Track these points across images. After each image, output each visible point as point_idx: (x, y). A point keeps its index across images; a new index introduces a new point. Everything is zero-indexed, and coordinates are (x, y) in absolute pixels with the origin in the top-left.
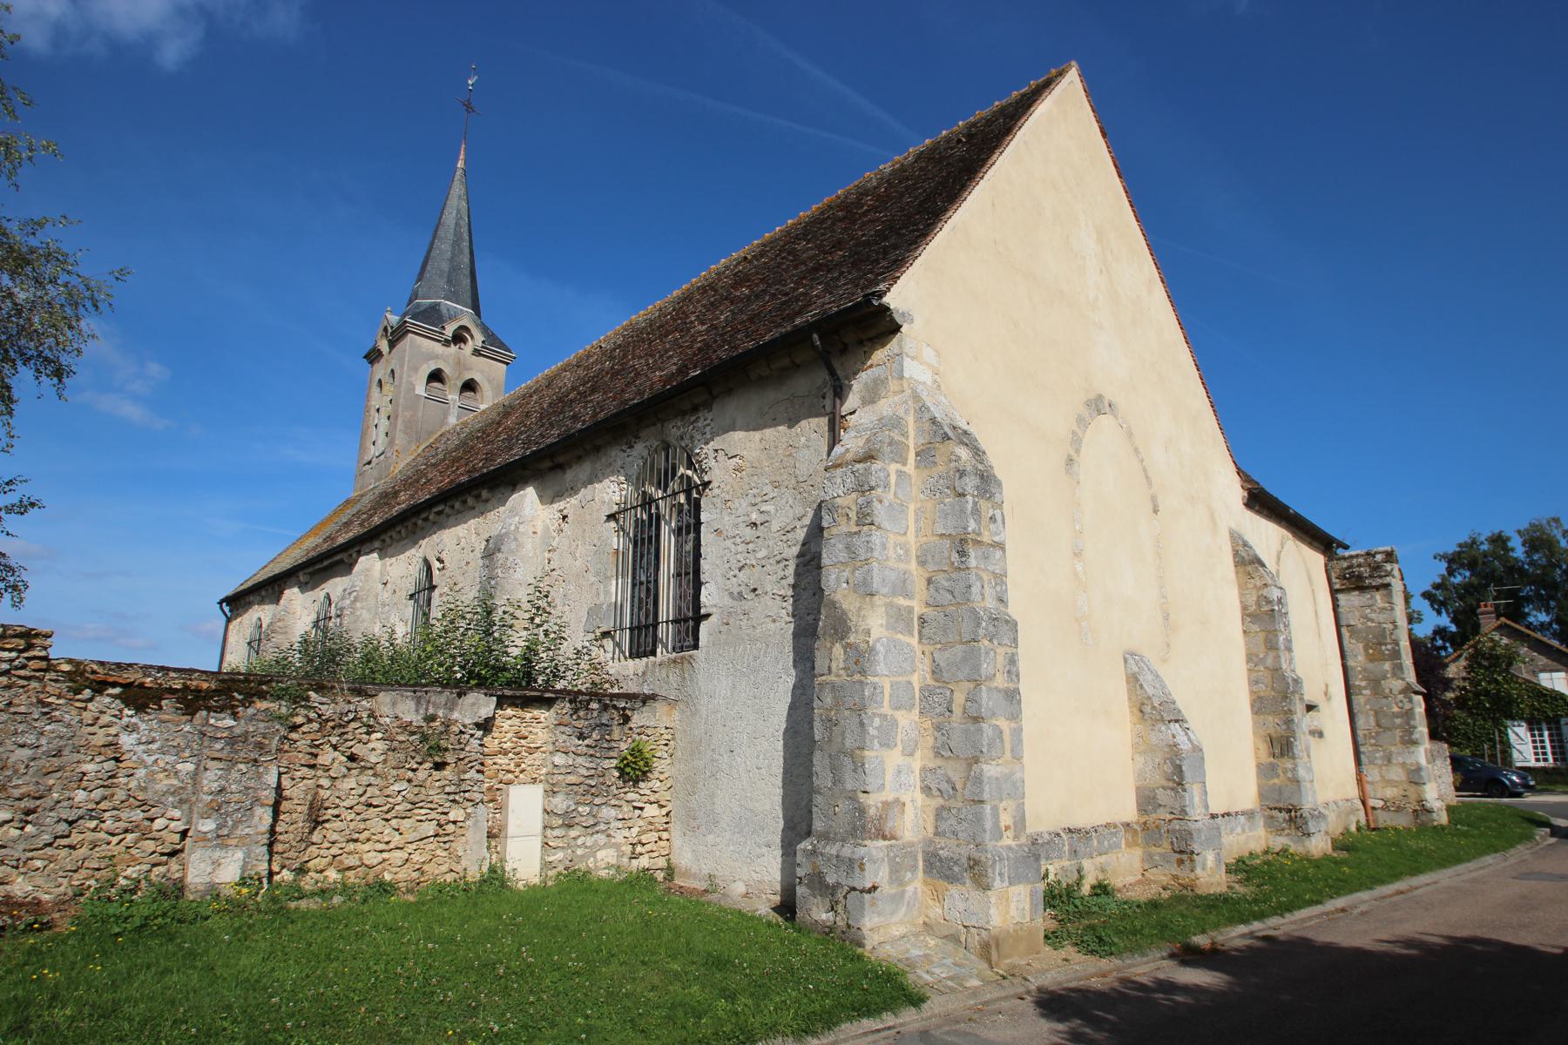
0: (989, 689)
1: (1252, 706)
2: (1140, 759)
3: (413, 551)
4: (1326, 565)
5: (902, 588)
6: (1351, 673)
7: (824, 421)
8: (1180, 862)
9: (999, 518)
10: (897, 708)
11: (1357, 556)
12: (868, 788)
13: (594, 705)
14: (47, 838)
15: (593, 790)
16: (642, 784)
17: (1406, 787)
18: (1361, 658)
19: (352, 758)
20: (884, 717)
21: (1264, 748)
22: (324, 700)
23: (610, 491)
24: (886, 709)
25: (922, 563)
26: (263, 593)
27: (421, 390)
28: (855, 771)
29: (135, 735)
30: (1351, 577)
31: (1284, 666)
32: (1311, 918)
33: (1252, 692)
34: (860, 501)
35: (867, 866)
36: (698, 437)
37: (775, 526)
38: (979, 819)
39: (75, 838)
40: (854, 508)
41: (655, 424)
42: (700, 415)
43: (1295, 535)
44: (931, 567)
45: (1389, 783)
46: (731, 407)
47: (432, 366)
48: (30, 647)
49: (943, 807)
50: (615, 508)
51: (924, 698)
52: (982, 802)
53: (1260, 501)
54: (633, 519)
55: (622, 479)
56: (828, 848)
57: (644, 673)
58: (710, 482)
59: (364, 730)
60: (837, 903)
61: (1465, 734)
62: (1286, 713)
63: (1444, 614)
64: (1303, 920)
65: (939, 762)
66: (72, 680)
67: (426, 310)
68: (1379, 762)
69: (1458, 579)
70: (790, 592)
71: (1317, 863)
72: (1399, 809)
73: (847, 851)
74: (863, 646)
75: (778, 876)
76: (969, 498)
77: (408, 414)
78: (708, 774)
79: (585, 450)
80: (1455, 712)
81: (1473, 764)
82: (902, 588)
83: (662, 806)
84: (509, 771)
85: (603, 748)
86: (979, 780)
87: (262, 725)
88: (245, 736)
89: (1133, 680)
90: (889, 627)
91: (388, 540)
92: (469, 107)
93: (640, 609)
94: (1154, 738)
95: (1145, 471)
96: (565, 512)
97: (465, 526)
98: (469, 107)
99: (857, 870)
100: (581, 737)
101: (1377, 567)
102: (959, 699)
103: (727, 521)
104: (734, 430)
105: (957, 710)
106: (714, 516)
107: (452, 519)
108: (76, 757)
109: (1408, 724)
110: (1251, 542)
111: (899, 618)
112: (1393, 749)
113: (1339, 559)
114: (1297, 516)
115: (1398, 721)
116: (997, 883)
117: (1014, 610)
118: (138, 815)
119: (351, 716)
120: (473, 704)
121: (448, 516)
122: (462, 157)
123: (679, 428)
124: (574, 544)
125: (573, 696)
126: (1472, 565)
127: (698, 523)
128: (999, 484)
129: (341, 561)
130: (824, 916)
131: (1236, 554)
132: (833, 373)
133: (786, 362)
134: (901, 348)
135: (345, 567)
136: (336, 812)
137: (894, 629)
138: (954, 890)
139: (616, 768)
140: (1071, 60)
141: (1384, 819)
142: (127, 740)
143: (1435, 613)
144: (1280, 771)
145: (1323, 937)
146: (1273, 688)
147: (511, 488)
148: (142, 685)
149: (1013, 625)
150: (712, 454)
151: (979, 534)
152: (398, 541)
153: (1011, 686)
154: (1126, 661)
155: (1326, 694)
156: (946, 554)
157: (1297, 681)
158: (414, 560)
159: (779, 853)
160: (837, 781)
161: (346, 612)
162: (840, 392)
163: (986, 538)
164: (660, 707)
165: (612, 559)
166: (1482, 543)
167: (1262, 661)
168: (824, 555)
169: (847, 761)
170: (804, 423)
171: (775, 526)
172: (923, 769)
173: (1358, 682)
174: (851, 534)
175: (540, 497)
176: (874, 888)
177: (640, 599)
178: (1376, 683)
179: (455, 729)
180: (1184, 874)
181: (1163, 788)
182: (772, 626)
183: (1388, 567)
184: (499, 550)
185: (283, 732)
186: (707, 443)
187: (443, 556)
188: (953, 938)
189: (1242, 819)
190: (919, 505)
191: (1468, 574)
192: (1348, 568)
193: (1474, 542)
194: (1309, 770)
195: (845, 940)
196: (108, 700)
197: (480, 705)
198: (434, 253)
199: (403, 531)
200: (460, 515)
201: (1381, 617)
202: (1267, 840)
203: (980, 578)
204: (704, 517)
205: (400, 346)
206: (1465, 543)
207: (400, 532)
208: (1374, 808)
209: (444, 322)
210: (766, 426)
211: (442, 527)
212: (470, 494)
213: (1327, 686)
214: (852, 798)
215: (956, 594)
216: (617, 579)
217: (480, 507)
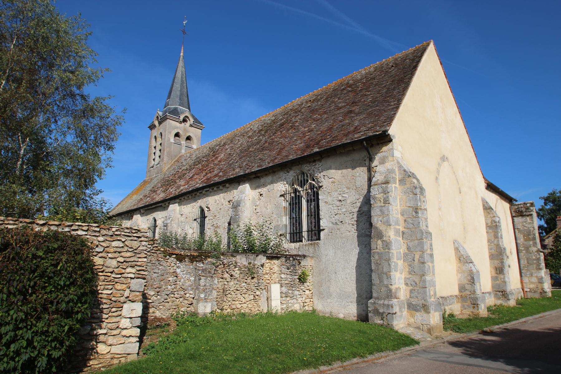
0: (426, 254)
1: (490, 257)
2: (460, 275)
3: (194, 204)
4: (510, 207)
5: (397, 223)
6: (519, 245)
7: (365, 169)
8: (474, 307)
9: (425, 201)
10: (398, 260)
11: (521, 204)
12: (392, 284)
13: (291, 259)
14: (163, 300)
15: (292, 286)
16: (305, 284)
17: (538, 284)
18: (522, 240)
19: (232, 276)
20: (395, 262)
21: (494, 271)
22: (224, 258)
23: (281, 187)
24: (395, 260)
25: (402, 215)
26: (123, 216)
27: (172, 140)
28: (387, 278)
29: (180, 269)
30: (519, 212)
31: (500, 244)
32: (516, 324)
33: (489, 252)
34: (385, 196)
35: (394, 307)
36: (316, 170)
37: (348, 201)
38: (425, 293)
39: (169, 300)
40: (382, 198)
41: (298, 165)
43: (500, 197)
44: (405, 216)
45: (532, 283)
46: (329, 162)
47: (176, 131)
48: (154, 243)
49: (412, 289)
50: (283, 193)
51: (404, 256)
52: (426, 288)
53: (491, 187)
55: (285, 183)
56: (379, 302)
57: (299, 248)
58: (322, 186)
59: (234, 267)
60: (384, 318)
61: (552, 265)
62: (501, 259)
63: (543, 220)
64: (514, 324)
65: (410, 276)
66: (164, 253)
67: (173, 111)
68: (528, 276)
69: (548, 207)
70: (355, 223)
71: (513, 308)
72: (535, 292)
73: (386, 302)
74: (388, 241)
75: (356, 311)
76: (418, 195)
77: (168, 149)
78: (327, 280)
80: (549, 257)
81: (556, 276)
82: (397, 223)
83: (310, 291)
84: (269, 280)
85: (294, 272)
86: (425, 281)
87: (209, 266)
88: (206, 269)
89: (457, 249)
90: (395, 235)
91: (183, 199)
92: (184, 32)
93: (293, 226)
94: (464, 268)
95: (457, 179)
96: (261, 193)
97: (218, 196)
98: (184, 32)
99: (390, 308)
100: (288, 269)
101: (527, 208)
102: (417, 257)
103: (329, 199)
104: (331, 169)
105: (416, 260)
106: (325, 197)
107: (212, 193)
108: (167, 276)
109: (538, 263)
110: (488, 201)
111: (397, 231)
112: (533, 271)
113: (514, 205)
114: (502, 191)
115: (535, 262)
116: (432, 312)
117: (430, 229)
118: (182, 293)
119: (231, 263)
120: (260, 259)
121: (211, 192)
122: (182, 51)
123: (308, 167)
124: (266, 204)
125: (286, 256)
126: (553, 202)
127: (318, 199)
128: (425, 190)
129: (161, 206)
130: (379, 322)
131: (484, 206)
132: (369, 154)
133: (351, 148)
134: (393, 147)
135: (165, 208)
136: (229, 292)
137: (396, 235)
138: (418, 314)
139: (298, 278)
140: (430, 39)
141: (529, 295)
142: (178, 271)
143: (539, 220)
144: (499, 279)
145: (523, 328)
146: (497, 251)
148: (181, 254)
149: (430, 234)
150: (322, 177)
151: (421, 206)
152: (187, 200)
153: (431, 253)
154: (454, 243)
155: (511, 252)
156: (411, 212)
157: (505, 249)
158: (195, 207)
159: (355, 304)
160: (381, 281)
161: (169, 225)
162: (371, 159)
163: (422, 208)
164: (309, 259)
165: (283, 210)
166: (557, 193)
167: (493, 242)
168: (372, 213)
169: (385, 276)
170: (358, 169)
171: (348, 201)
172: (405, 278)
173: (521, 248)
174: (381, 206)
175: (251, 187)
176: (396, 313)
177: (293, 224)
178: (527, 249)
179: (256, 267)
180: (475, 311)
181: (468, 284)
182: (349, 233)
183: (532, 208)
184: (239, 206)
185: (215, 268)
186: (320, 173)
187: (209, 206)
188: (418, 328)
189: (487, 294)
190: (400, 197)
191: (552, 205)
192: (517, 208)
193: (554, 193)
194: (509, 278)
195: (389, 327)
196: (173, 259)
197: (262, 259)
198: (174, 88)
199: (190, 197)
200: (215, 192)
201: (529, 226)
202: (495, 301)
203: (422, 220)
204: (320, 197)
205: (163, 124)
206: (551, 193)
207: (189, 197)
208: (526, 292)
209: (179, 114)
210: (343, 169)
211: (208, 196)
213: (511, 250)
214: (387, 286)
215: (415, 225)
217: (225, 189)
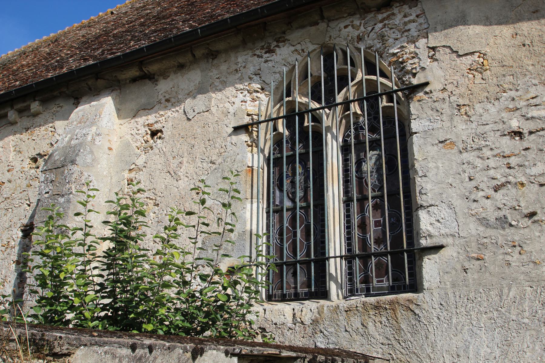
42: (396, 11)
54: (270, 135)
79: (194, 56)
96: (157, 127)
147: (72, 101)
150: (424, 53)
175: (118, 110)
212: (12, 108)
216: (252, 203)
217: (25, 121)
